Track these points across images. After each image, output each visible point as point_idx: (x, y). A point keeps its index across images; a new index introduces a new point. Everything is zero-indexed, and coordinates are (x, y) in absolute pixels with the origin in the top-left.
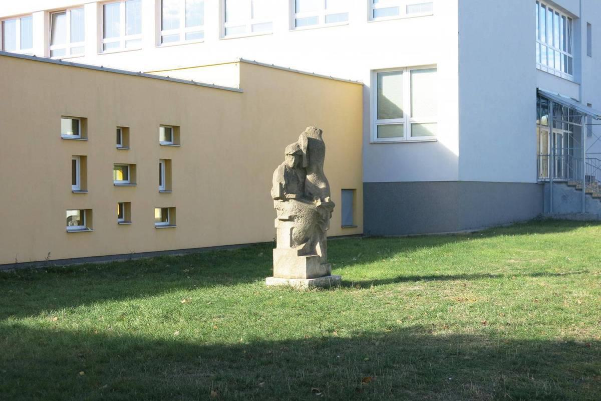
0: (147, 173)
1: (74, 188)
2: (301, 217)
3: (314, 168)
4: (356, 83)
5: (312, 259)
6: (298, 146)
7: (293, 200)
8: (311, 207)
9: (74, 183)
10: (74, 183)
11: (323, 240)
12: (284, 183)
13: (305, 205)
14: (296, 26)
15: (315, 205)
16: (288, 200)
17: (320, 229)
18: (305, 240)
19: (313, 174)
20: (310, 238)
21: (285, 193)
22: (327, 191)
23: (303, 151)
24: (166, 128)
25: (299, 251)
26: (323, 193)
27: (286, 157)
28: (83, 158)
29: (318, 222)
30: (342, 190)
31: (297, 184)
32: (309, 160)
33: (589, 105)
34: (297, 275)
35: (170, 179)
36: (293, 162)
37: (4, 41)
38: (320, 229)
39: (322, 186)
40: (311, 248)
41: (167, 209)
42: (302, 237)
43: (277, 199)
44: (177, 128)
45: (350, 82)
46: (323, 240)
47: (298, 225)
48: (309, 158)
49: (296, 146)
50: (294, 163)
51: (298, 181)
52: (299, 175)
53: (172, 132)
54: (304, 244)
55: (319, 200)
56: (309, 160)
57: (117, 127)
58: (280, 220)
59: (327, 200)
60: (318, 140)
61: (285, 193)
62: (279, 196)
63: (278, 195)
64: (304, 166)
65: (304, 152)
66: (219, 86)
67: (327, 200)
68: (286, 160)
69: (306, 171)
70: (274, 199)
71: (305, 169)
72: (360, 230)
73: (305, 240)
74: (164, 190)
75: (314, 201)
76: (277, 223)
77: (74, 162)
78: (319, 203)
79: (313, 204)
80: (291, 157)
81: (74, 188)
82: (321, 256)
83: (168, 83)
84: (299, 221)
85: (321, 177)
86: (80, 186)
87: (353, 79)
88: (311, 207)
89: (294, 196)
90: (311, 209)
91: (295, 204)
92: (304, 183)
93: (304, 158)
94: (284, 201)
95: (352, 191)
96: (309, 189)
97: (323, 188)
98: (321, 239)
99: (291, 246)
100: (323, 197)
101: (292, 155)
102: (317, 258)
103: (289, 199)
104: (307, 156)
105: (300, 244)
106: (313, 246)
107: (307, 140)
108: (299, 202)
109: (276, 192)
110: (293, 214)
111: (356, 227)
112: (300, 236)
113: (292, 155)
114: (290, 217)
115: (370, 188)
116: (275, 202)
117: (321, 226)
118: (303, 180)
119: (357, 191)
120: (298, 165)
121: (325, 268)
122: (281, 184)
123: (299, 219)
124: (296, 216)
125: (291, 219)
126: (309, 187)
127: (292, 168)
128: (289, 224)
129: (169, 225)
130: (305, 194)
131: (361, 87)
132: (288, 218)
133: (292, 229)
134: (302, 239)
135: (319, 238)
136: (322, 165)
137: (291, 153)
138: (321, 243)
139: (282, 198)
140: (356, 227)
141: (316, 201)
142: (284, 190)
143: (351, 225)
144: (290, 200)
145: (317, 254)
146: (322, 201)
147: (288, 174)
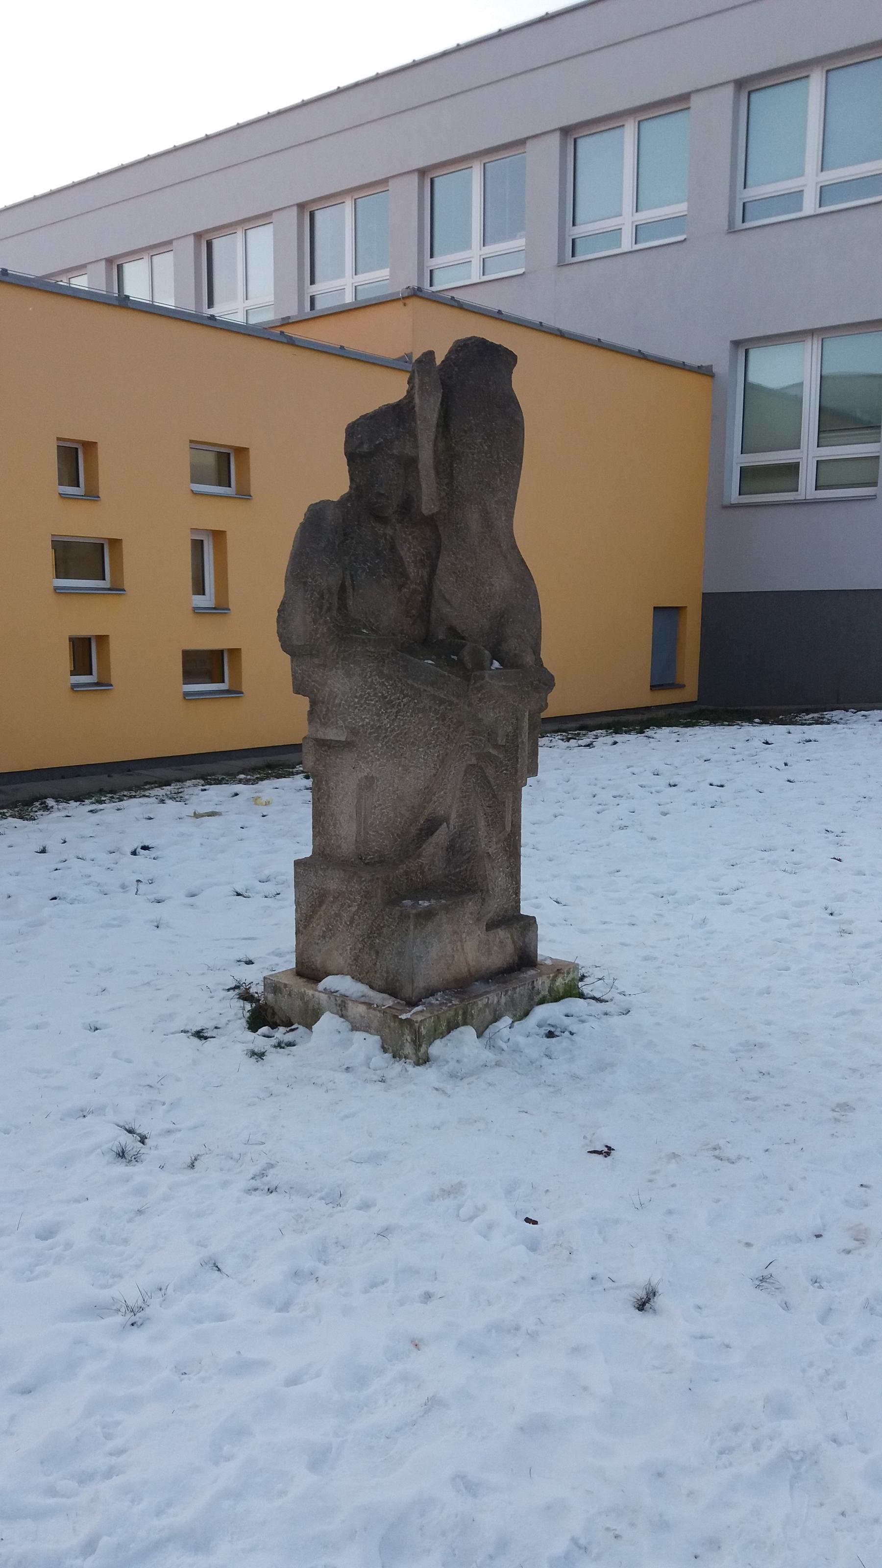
0: (154, 566)
1: (200, 601)
9: (199, 589)
10: (199, 589)
14: (745, 188)
20: (447, 820)
28: (218, 536)
30: (656, 609)
33: (615, 743)
37: (383, 369)
41: (222, 652)
48: (451, 476)
57: (58, 439)
66: (378, 297)
71: (431, 521)
77: (198, 546)
81: (200, 601)
86: (213, 598)
93: (423, 473)
95: (677, 610)
96: (446, 610)
115: (715, 604)
118: (425, 572)
126: (448, 602)
136: (509, 504)
140: (682, 686)
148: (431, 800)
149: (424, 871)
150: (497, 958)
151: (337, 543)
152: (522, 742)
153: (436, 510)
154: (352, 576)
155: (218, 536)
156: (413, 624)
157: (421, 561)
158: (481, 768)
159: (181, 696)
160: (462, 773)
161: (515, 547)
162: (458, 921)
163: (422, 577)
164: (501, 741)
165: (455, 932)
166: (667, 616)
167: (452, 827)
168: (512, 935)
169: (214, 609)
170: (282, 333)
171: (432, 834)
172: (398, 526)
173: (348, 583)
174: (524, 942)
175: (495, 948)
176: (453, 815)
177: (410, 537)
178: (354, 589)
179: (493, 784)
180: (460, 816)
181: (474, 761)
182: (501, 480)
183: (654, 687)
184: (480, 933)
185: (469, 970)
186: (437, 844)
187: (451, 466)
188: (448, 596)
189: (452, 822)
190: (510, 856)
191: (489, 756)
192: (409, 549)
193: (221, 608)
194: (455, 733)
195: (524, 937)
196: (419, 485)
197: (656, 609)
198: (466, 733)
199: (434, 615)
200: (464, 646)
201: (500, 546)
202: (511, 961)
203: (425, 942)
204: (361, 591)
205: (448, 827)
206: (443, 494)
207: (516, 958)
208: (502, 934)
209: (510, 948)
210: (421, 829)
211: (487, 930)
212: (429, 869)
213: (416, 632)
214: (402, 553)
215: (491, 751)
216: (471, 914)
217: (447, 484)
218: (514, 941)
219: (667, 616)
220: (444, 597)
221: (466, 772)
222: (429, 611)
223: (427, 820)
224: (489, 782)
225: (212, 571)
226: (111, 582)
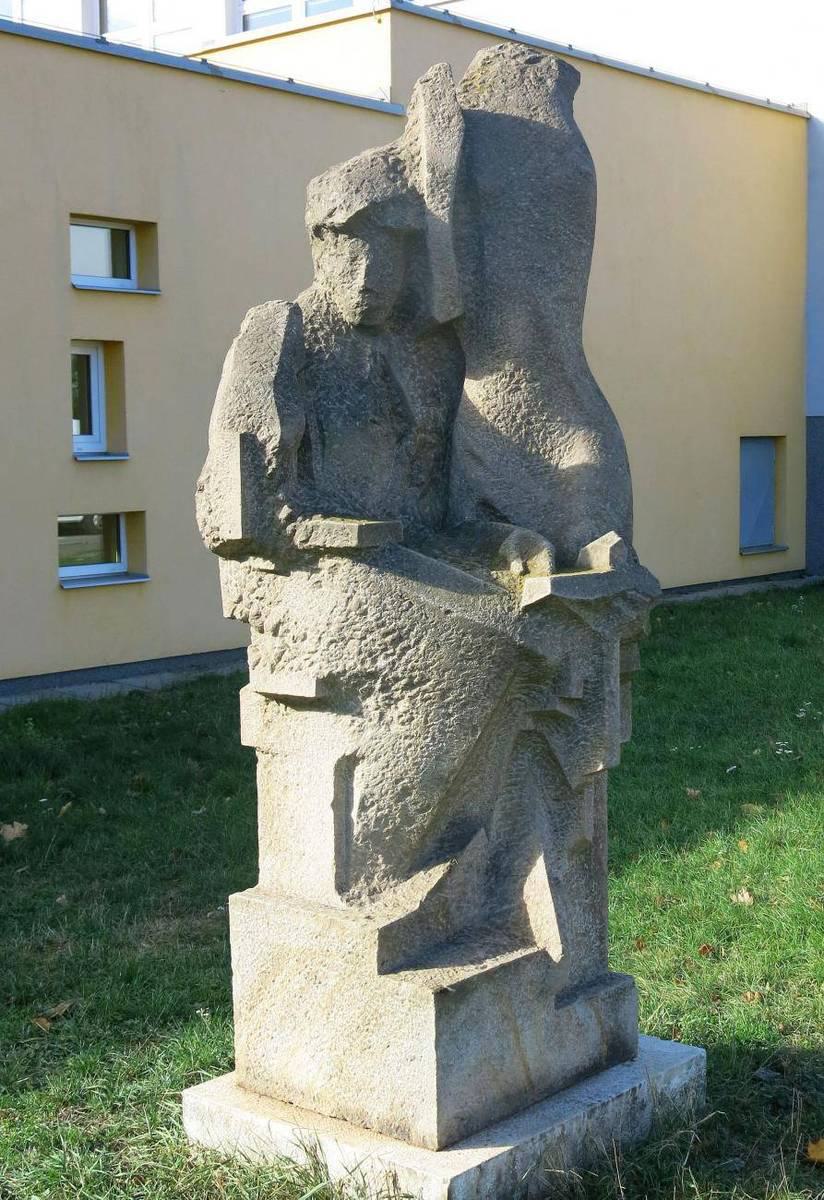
2: (410, 686)
3: (515, 326)
4: (788, 113)
5: (484, 994)
6: (395, 168)
7: (344, 564)
8: (478, 610)
11: (572, 839)
12: (271, 434)
13: (433, 598)
15: (510, 593)
16: (306, 559)
17: (550, 762)
18: (447, 840)
19: (508, 367)
20: (485, 823)
21: (284, 512)
22: (610, 493)
23: (431, 204)
24: (114, 232)
25: (387, 935)
26: (580, 506)
27: (317, 248)
28: (112, 348)
29: (539, 716)
30: (742, 438)
31: (388, 435)
32: (479, 272)
34: (378, 1110)
35: (122, 412)
36: (360, 281)
38: (550, 762)
39: (574, 453)
40: (490, 893)
41: (117, 516)
42: (422, 820)
43: (235, 551)
44: (146, 228)
45: (766, 107)
46: (572, 839)
47: (388, 740)
48: (480, 260)
49: (382, 166)
50: (365, 291)
51: (400, 412)
52: (410, 382)
53: (130, 242)
54: (438, 872)
55: (542, 561)
56: (479, 272)
58: (271, 697)
59: (600, 554)
60: (545, 129)
61: (284, 512)
62: (237, 534)
63: (232, 528)
64: (441, 317)
65: (438, 208)
67: (600, 554)
68: (320, 276)
69: (457, 349)
70: (218, 551)
71: (448, 330)
72: (795, 557)
73: (447, 840)
74: (103, 449)
75: (505, 564)
76: (255, 724)
77: (81, 365)
78: (536, 584)
79: (491, 588)
80: (346, 245)
82: (556, 953)
83: (101, 61)
84: (392, 714)
85: (567, 387)
87: (781, 97)
88: (478, 610)
89: (343, 531)
90: (478, 630)
91: (361, 594)
92: (446, 435)
93: (434, 256)
94: (282, 570)
95: (775, 441)
96: (476, 473)
97: (577, 471)
98: (559, 830)
99: (342, 887)
100: (575, 532)
101: (349, 229)
102: (530, 972)
103: (319, 553)
104: (457, 239)
105: (425, 864)
106: (503, 877)
107: (457, 123)
108: (391, 581)
109: (221, 508)
110: (349, 661)
111: (784, 550)
112: (408, 820)
113: (349, 229)
114: (328, 683)
116: (228, 569)
117: (557, 742)
118: (439, 413)
119: (789, 442)
120: (394, 306)
121: (592, 1023)
122: (250, 445)
123: (391, 701)
124: (373, 676)
125: (335, 695)
127: (360, 327)
128: (332, 734)
129: (126, 575)
130: (439, 523)
131: (803, 123)
132: (310, 692)
133: (346, 768)
134: (424, 833)
135: (542, 826)
136: (575, 302)
137: (340, 218)
138: (566, 864)
139: (265, 541)
140: (784, 550)
141: (516, 566)
142: (287, 487)
143: (770, 545)
144: (325, 563)
145: (527, 940)
146: (564, 560)
147: (304, 371)
148: (458, 791)
149: (448, 913)
150: (578, 1051)
151: (296, 371)
152: (611, 692)
153: (456, 314)
154: (320, 423)
155: (112, 348)
156: (423, 495)
157: (434, 395)
158: (540, 735)
159: (56, 584)
160: (510, 746)
161: (586, 372)
162: (510, 999)
163: (435, 420)
164: (576, 692)
165: (505, 1017)
166: (760, 447)
167: (493, 833)
168: (597, 1011)
169: (106, 454)
170: (204, 61)
171: (463, 847)
172: (395, 339)
173: (313, 436)
174: (616, 1020)
175: (571, 1035)
176: (497, 815)
177: (414, 357)
178: (323, 444)
179: (562, 763)
180: (507, 816)
181: (530, 724)
182: (562, 265)
183: (745, 552)
184: (545, 1013)
185: (528, 1077)
186: (470, 865)
187: (480, 244)
188: (479, 451)
189: (494, 827)
190: (591, 877)
191: (556, 717)
192: (413, 376)
193: (115, 454)
194: (497, 682)
195: (615, 1010)
196: (428, 275)
197: (742, 438)
198: (517, 679)
199: (456, 481)
200: (508, 533)
201: (562, 370)
202: (596, 1054)
203: (456, 1040)
204: (336, 446)
205: (487, 835)
206: (469, 289)
207: (605, 1048)
208: (580, 1009)
209: (594, 1035)
210: (442, 841)
211: (557, 1007)
212: (459, 908)
213: (427, 510)
214: (403, 384)
215: (558, 708)
216: (531, 983)
217: (474, 273)
218: (600, 1023)
219: (760, 447)
220: (474, 456)
221: (516, 742)
222: (447, 475)
223: (452, 824)
224: (555, 761)
225: (103, 402)
226: (139, 283)
